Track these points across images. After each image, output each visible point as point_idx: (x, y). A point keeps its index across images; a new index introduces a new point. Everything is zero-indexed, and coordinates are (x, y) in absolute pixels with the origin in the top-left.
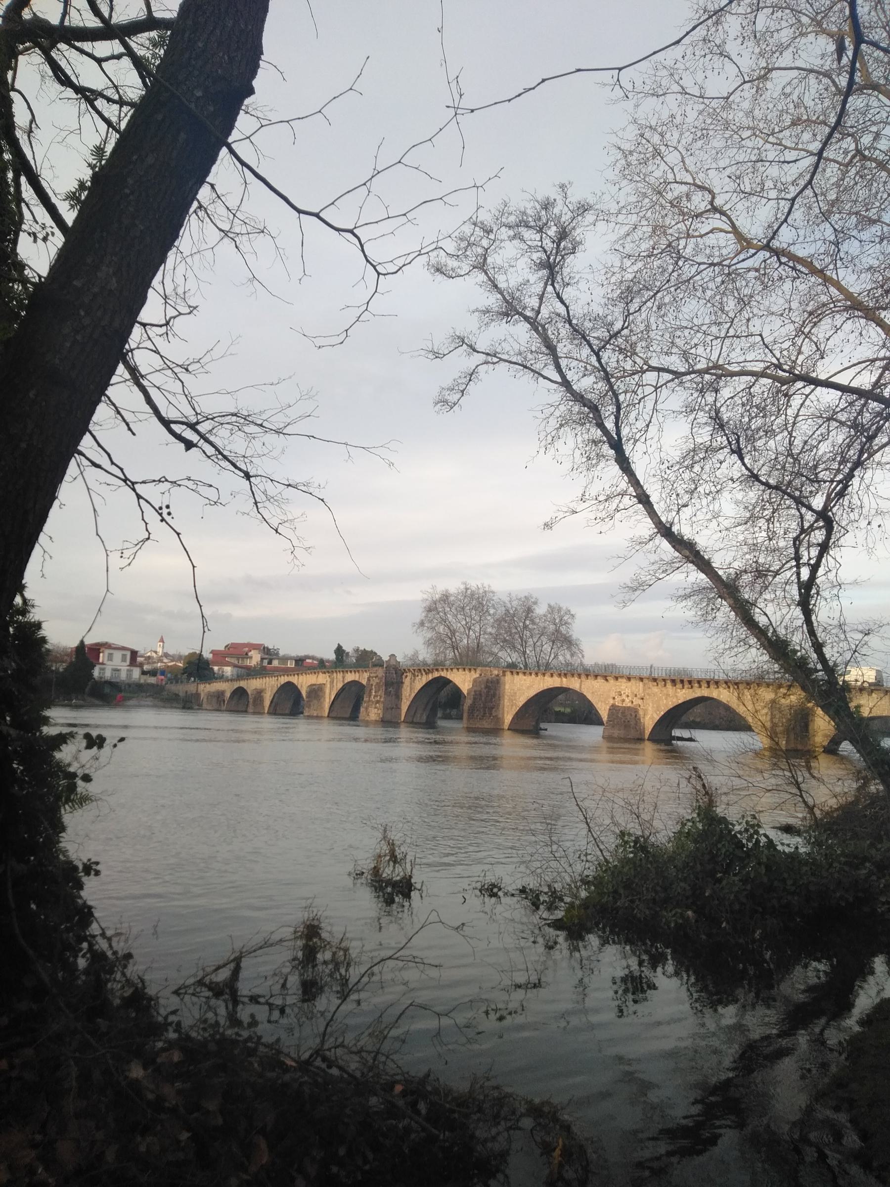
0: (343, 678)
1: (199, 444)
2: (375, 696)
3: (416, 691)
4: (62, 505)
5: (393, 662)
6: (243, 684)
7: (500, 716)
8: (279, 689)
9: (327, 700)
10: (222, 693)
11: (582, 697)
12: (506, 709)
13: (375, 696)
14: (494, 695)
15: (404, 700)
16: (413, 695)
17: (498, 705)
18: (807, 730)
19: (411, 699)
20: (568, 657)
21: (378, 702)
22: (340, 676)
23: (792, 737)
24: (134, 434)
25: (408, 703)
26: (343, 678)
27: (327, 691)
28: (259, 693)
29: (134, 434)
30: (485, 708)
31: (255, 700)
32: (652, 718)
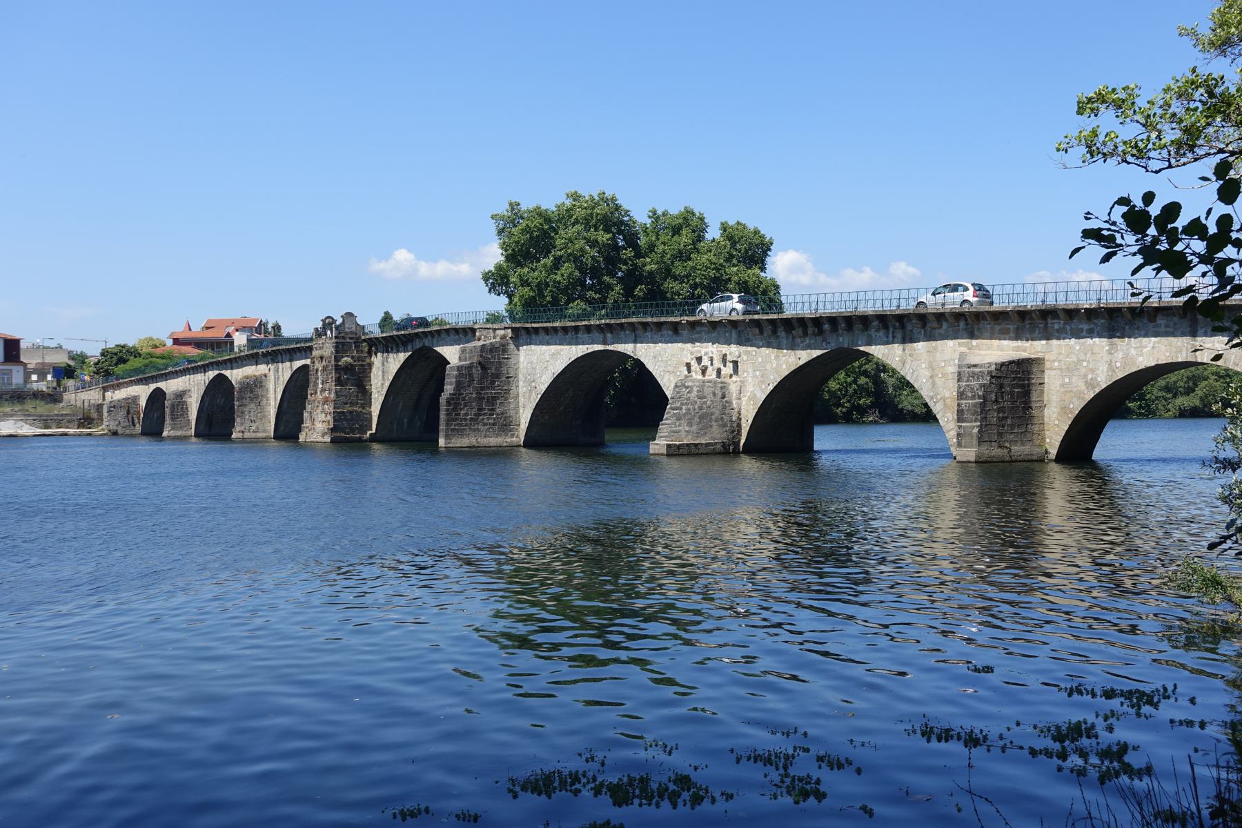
0: (291, 367)
1: (1206, 346)
2: (323, 390)
3: (391, 378)
4: (1090, 385)
5: (349, 327)
6: (162, 385)
7: (512, 413)
8: (208, 388)
9: (272, 403)
10: (135, 399)
11: (639, 364)
12: (521, 399)
13: (323, 390)
14: (497, 375)
15: (374, 396)
16: (387, 384)
17: (508, 392)
18: (1027, 406)
19: (384, 393)
20: (624, 267)
21: (326, 401)
22: (288, 364)
23: (993, 417)
24: (1070, 257)
25: (381, 399)
26: (291, 367)
27: (271, 386)
28: (181, 395)
29: (1070, 257)
30: (480, 399)
31: (173, 407)
32: (752, 398)
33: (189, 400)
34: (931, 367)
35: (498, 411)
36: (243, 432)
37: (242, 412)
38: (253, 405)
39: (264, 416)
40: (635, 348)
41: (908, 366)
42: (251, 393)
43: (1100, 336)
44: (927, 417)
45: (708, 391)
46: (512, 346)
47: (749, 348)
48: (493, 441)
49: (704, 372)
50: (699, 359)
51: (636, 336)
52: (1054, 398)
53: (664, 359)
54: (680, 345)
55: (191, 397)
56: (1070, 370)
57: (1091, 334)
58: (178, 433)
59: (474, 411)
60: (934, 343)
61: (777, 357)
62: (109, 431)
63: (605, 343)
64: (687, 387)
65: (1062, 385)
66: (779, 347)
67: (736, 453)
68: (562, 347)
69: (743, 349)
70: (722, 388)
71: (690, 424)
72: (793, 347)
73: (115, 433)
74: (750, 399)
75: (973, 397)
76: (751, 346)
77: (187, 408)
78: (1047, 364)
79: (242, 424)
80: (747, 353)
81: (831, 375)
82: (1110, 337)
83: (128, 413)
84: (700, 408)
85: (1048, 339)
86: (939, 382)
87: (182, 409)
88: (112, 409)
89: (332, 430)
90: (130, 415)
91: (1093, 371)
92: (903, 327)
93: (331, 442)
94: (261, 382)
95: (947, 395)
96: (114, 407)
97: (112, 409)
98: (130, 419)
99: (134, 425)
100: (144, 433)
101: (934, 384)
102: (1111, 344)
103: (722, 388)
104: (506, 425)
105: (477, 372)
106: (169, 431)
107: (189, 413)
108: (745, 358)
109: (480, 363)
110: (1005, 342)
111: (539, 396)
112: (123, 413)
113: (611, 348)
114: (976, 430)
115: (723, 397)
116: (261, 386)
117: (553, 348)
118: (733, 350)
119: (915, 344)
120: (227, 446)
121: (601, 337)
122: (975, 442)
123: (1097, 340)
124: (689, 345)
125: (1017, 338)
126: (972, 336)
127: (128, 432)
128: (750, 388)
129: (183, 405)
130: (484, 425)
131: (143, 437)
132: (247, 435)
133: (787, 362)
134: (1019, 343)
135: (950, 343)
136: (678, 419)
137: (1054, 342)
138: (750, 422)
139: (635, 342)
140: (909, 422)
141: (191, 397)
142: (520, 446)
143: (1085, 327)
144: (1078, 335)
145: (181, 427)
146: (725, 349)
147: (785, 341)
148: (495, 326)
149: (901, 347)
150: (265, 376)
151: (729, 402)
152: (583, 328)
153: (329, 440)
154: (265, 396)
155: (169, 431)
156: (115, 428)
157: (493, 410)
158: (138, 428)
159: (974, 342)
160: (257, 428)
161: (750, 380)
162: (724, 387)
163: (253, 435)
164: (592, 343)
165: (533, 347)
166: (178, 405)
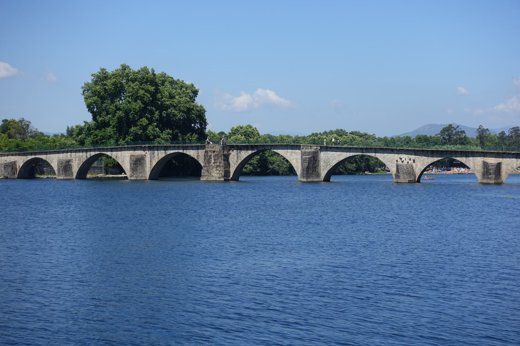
14: (316, 160)
32: (420, 169)
33: (72, 164)
34: (474, 163)
35: (317, 171)
36: (137, 177)
37: (136, 169)
38: (140, 167)
39: (145, 171)
40: (375, 155)
41: (467, 163)
42: (140, 162)
43: (514, 158)
44: (296, 175)
45: (408, 167)
46: (319, 152)
47: (418, 156)
48: (316, 180)
49: (403, 162)
50: (401, 159)
51: (376, 151)
52: (504, 171)
53: (387, 158)
54: (393, 155)
55: (73, 162)
56: (508, 165)
57: (512, 158)
58: (68, 178)
59: (312, 171)
60: (474, 158)
61: (427, 159)
62: (5, 176)
63: (362, 152)
64: (402, 166)
65: (506, 168)
66: (428, 156)
67: (415, 182)
68: (343, 153)
69: (416, 156)
70: (412, 166)
71: (407, 175)
72: (433, 157)
73: (7, 178)
74: (419, 169)
75: (493, 170)
76: (419, 156)
77: (71, 167)
78: (503, 163)
79: (136, 174)
80: (418, 158)
81: (93, 162)
82: (517, 158)
83: (12, 168)
84: (408, 171)
85: (503, 158)
86: (476, 166)
87: (69, 167)
88: (6, 167)
89: (224, 176)
90: (13, 170)
91: (513, 165)
92: (466, 154)
93: (224, 180)
94: (143, 158)
95: (478, 169)
96: (6, 166)
97: (6, 167)
98: (13, 171)
99: (14, 174)
100: (18, 178)
101: (474, 167)
102: (517, 160)
103: (412, 166)
104: (318, 175)
105: (312, 159)
106: (64, 177)
107: (72, 169)
108: (417, 159)
109: (313, 157)
110: (493, 158)
111: (331, 167)
112: (10, 169)
113: (102, 153)
114: (494, 177)
115: (412, 168)
116: (143, 159)
117: (338, 153)
118: (413, 157)
119: (469, 158)
120: (328, 183)
121: (361, 151)
122: (494, 179)
123: (5, 157)
124: (397, 155)
125: (495, 158)
126: (484, 157)
127: (12, 177)
128: (419, 166)
129: (70, 166)
130: (314, 175)
131: (19, 180)
132: (138, 178)
133: (430, 160)
134: (496, 159)
135: (479, 158)
136: (404, 174)
137: (504, 159)
138: (419, 175)
139: (376, 153)
140: (272, 175)
141: (73, 162)
142: (322, 181)
143: (511, 156)
144: (510, 158)
145: (69, 175)
146: (410, 156)
147: (430, 155)
148: (312, 145)
149: (465, 158)
150: (145, 155)
151: (414, 170)
152: (250, 146)
153: (223, 180)
154: (145, 163)
155: (64, 177)
156: (7, 175)
157: (316, 170)
158: (16, 176)
159: (485, 158)
160: (142, 176)
161: (419, 164)
162: (412, 166)
163: (141, 178)
164: (357, 152)
165: (328, 152)
166: (68, 166)
